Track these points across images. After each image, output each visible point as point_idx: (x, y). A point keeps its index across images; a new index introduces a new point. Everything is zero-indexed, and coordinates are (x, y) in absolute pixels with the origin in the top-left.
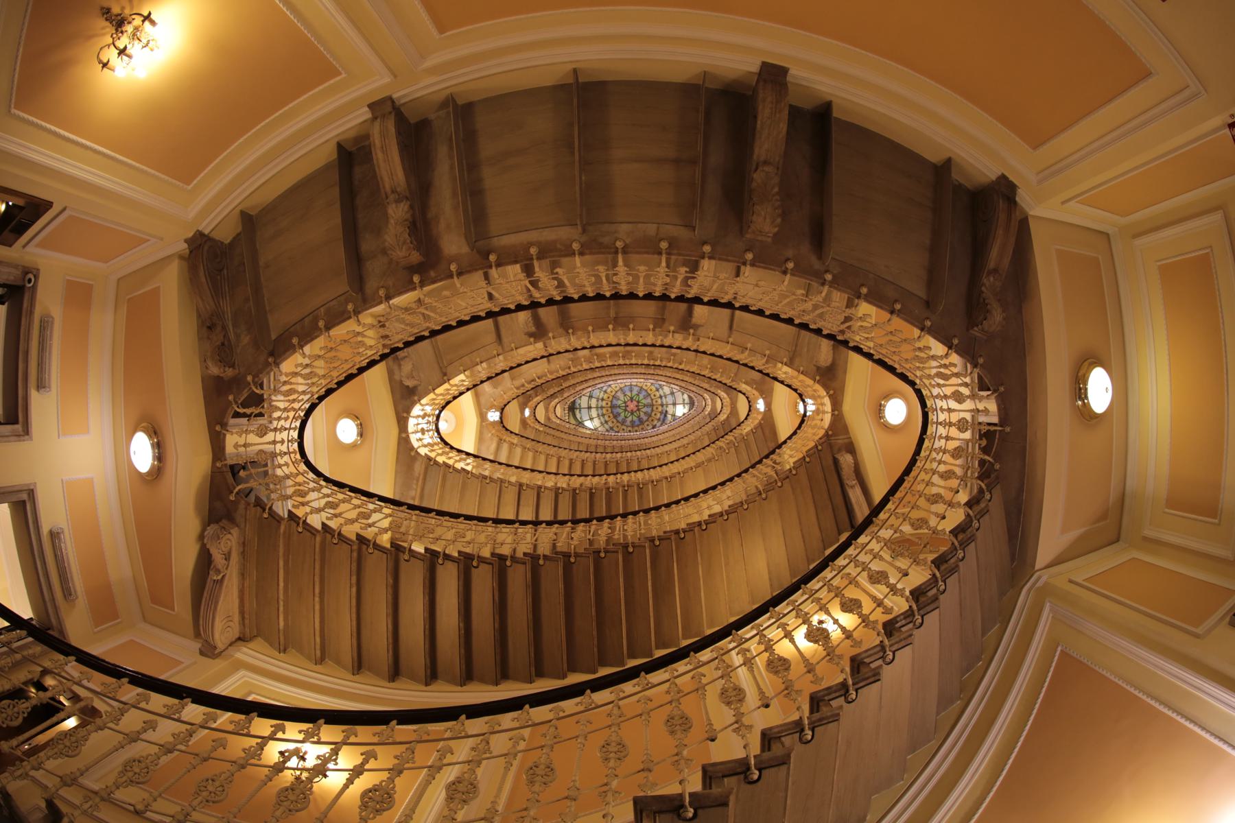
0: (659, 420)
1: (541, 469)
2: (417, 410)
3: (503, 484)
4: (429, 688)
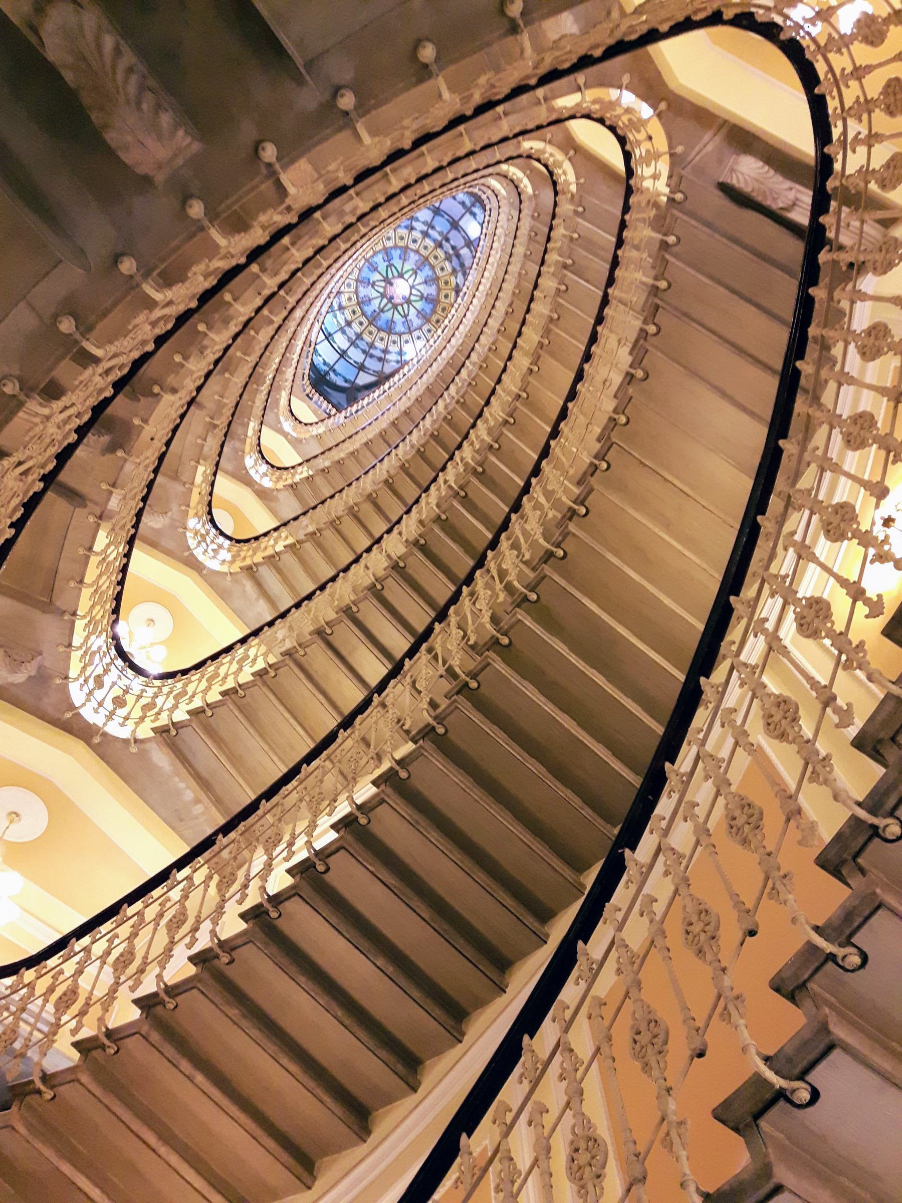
0: (454, 271)
1: (331, 573)
2: (77, 694)
3: (297, 656)
4: (422, 1090)
